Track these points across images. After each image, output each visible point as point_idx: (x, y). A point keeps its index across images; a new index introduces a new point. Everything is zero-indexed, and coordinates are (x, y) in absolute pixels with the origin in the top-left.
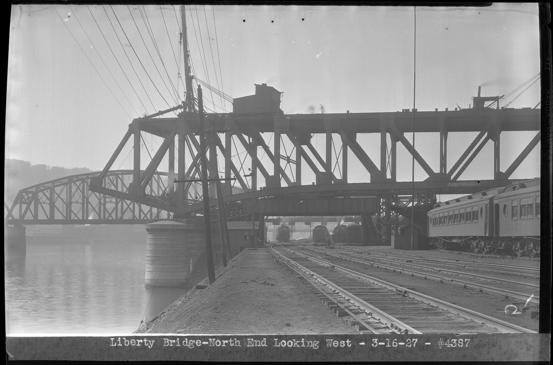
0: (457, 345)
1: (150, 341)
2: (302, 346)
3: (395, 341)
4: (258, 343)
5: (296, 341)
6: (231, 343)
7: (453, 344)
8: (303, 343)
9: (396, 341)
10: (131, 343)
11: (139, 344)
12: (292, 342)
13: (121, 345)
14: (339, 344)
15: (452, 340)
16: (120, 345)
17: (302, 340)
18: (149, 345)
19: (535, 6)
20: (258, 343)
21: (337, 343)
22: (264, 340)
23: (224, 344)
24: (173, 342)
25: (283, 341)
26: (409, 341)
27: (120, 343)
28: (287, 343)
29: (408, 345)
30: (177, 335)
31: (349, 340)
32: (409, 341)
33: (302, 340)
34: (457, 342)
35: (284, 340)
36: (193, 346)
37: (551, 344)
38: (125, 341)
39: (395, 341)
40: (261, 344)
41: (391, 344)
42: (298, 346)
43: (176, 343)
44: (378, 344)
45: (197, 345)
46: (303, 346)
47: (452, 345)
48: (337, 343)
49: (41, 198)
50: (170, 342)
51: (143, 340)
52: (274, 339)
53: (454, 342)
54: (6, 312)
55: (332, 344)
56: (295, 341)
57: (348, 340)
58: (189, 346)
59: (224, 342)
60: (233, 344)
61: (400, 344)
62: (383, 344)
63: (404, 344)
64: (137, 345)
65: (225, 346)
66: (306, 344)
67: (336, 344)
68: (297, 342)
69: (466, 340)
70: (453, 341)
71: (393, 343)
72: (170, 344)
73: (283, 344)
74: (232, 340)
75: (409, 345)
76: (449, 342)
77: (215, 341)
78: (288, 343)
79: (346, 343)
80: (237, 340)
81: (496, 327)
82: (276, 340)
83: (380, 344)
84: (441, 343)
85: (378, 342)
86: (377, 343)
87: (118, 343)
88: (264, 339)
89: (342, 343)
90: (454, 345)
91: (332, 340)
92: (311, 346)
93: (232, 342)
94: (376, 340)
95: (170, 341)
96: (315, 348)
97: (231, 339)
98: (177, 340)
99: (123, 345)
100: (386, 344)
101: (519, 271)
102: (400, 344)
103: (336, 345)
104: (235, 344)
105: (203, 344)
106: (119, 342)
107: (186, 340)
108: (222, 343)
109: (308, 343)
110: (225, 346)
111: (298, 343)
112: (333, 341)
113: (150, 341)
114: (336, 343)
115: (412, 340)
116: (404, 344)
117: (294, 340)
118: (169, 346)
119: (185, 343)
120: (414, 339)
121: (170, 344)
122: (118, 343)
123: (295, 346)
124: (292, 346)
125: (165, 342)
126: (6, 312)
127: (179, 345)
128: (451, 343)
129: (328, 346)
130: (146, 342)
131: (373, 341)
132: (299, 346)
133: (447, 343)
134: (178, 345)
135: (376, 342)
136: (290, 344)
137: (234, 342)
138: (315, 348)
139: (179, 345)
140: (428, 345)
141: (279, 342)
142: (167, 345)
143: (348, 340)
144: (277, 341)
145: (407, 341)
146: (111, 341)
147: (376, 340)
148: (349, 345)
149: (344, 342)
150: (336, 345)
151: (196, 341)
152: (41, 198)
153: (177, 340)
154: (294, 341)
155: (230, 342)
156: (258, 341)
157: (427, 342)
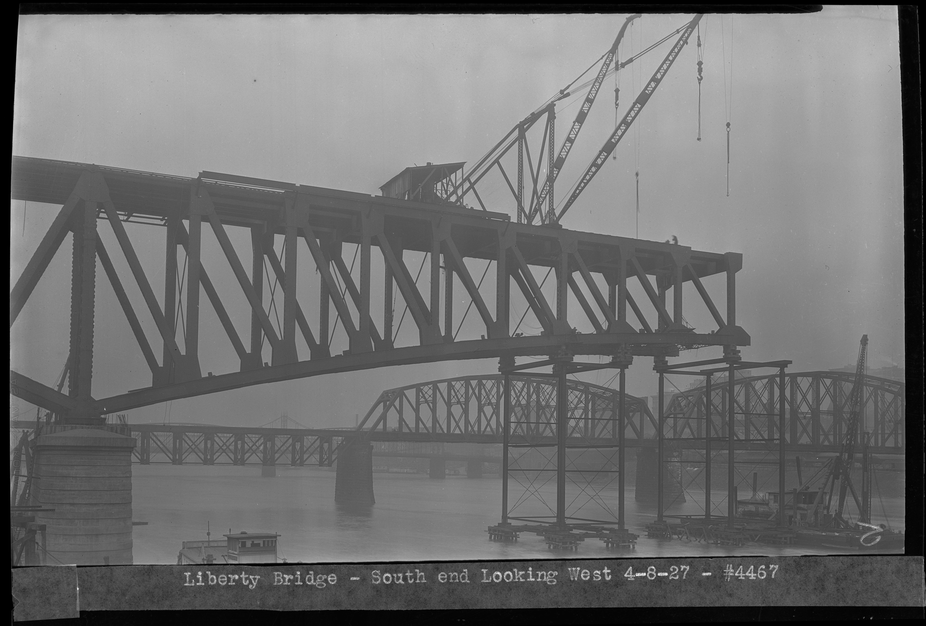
4: (542, 575)
6: (244, 580)
14: (592, 576)
18: (251, 582)
19: (893, 11)
21: (445, 576)
22: (311, 574)
23: (287, 580)
24: (235, 578)
26: (674, 570)
28: (217, 579)
31: (608, 570)
35: (497, 571)
37: (925, 571)
39: (762, 569)
40: (393, 577)
42: (522, 580)
45: (330, 582)
48: (334, 577)
49: (458, 391)
55: (579, 575)
57: (606, 568)
58: (316, 584)
60: (413, 580)
64: (198, 584)
67: (585, 575)
68: (521, 573)
69: (683, 567)
72: (284, 581)
73: (497, 577)
74: (245, 574)
75: (675, 575)
76: (752, 570)
77: (580, 572)
79: (603, 575)
84: (629, 575)
91: (578, 569)
93: (246, 579)
95: (285, 576)
96: (319, 587)
97: (243, 573)
98: (529, 570)
103: (333, 581)
109: (467, 578)
112: (580, 572)
115: (680, 568)
118: (282, 585)
122: (198, 581)
128: (681, 573)
130: (411, 576)
133: (629, 574)
134: (299, 583)
138: (319, 587)
140: (708, 577)
141: (490, 574)
143: (606, 568)
146: (186, 578)
149: (400, 575)
152: (458, 391)
156: (542, 573)
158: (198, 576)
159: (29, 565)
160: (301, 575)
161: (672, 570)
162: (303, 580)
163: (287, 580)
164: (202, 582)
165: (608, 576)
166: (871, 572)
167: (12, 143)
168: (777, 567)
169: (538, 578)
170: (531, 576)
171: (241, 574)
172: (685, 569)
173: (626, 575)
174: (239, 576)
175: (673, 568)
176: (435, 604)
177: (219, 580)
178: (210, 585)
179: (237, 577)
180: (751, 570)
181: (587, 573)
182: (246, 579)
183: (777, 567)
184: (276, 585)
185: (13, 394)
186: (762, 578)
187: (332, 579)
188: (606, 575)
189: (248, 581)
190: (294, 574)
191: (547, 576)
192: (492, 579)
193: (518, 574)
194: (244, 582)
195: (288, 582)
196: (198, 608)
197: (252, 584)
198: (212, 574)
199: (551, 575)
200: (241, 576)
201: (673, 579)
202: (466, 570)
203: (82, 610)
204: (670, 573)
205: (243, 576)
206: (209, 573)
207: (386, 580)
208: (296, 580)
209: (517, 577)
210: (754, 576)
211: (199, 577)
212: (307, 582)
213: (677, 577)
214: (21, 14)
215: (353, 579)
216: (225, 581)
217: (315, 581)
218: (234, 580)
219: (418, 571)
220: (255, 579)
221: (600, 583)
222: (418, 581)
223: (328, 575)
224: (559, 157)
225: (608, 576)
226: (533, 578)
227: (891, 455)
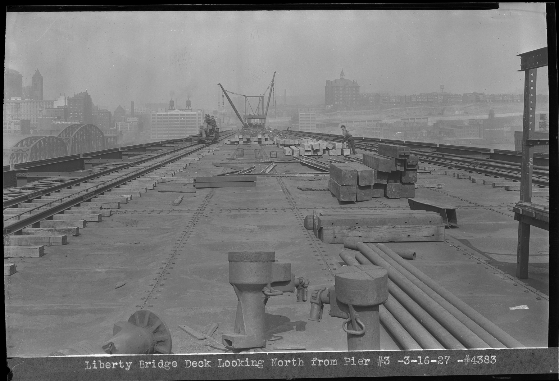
1: (127, 363)
5: (207, 360)
6: (121, 365)
8: (420, 359)
10: (193, 364)
13: (96, 368)
15: (478, 357)
16: (95, 368)
17: (352, 358)
21: (195, 363)
25: (228, 361)
31: (295, 360)
32: (441, 358)
33: (352, 358)
34: (483, 358)
36: (169, 368)
39: (427, 359)
40: (330, 362)
42: (242, 366)
43: (352, 362)
46: (248, 365)
48: (195, 363)
50: (145, 364)
51: (118, 363)
53: (494, 359)
56: (239, 361)
59: (114, 364)
61: (432, 361)
62: (416, 361)
64: (112, 368)
66: (250, 363)
68: (208, 362)
69: (446, 357)
71: (425, 361)
72: (145, 366)
73: (227, 364)
77: (277, 361)
80: (300, 360)
82: (220, 360)
83: (412, 361)
85: (410, 359)
86: (409, 360)
90: (407, 362)
92: (256, 365)
94: (408, 357)
100: (418, 362)
101: (429, 290)
102: (432, 361)
103: (194, 365)
105: (431, 362)
106: (94, 365)
107: (161, 362)
108: (285, 363)
111: (243, 363)
113: (127, 363)
115: (444, 357)
119: (160, 365)
120: (493, 356)
123: (239, 366)
128: (444, 361)
131: (405, 358)
136: (234, 364)
139: (249, 366)
142: (428, 363)
144: (88, 363)
147: (408, 357)
148: (295, 364)
150: (194, 365)
151: (171, 363)
157: (432, 360)
158: (93, 363)
159: (12, 357)
161: (439, 358)
162: (156, 365)
163: (366, 362)
164: (96, 367)
166: (517, 361)
167: (526, 2)
168: (449, 357)
171: (119, 362)
172: (447, 358)
174: (291, 361)
175: (440, 358)
176: (343, 375)
177: (106, 365)
179: (116, 364)
180: (474, 359)
182: (122, 365)
183: (449, 357)
184: (87, 370)
185: (547, 217)
195: (367, 363)
196: (276, 378)
198: (101, 362)
199: (167, 364)
202: (495, 356)
204: (438, 360)
208: (152, 364)
209: (239, 364)
211: (408, 360)
212: (425, 363)
213: (443, 363)
214: (8, 12)
216: (109, 366)
218: (148, 365)
219: (299, 358)
220: (129, 364)
224: (200, 144)
226: (96, 367)
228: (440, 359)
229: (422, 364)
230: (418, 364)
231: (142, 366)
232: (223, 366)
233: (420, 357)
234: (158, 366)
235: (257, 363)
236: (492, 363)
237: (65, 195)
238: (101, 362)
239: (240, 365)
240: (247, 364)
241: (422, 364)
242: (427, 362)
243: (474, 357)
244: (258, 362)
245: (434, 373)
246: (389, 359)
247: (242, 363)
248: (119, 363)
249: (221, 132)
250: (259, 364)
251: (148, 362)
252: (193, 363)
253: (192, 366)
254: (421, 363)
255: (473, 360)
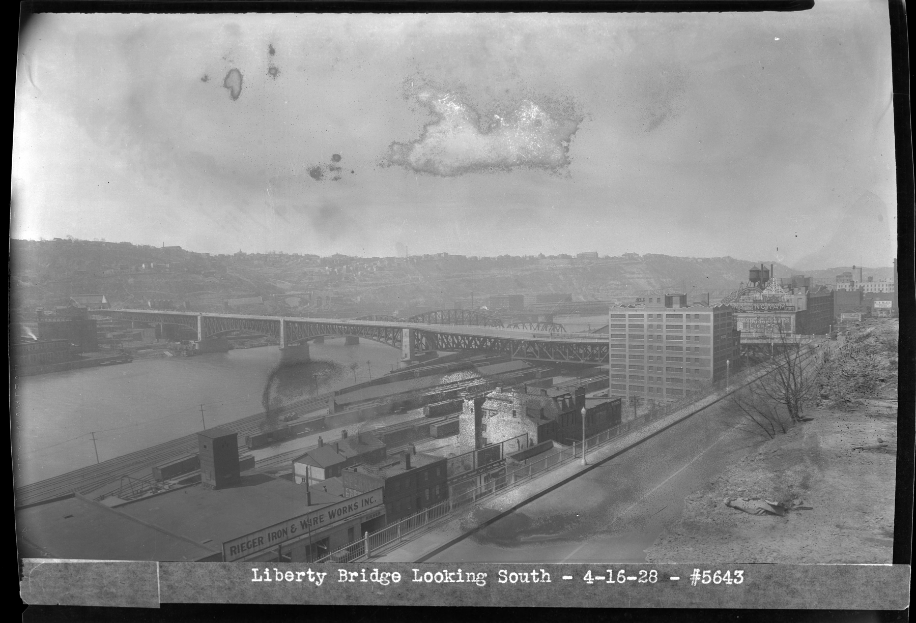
0: (508, 581)
1: (318, 574)
2: (458, 581)
3: (717, 574)
4: (471, 576)
7: (737, 578)
9: (720, 575)
11: (352, 578)
12: (292, 575)
16: (268, 580)
18: (317, 579)
20: (471, 576)
27: (364, 577)
28: (284, 575)
29: (642, 579)
30: (77, 560)
32: (644, 574)
33: (458, 572)
36: (387, 582)
38: (277, 573)
40: (519, 576)
41: (614, 578)
42: (452, 581)
43: (360, 577)
44: (626, 578)
47: (735, 581)
50: (349, 576)
52: (413, 570)
54: (234, 30)
58: (380, 581)
60: (538, 580)
62: (603, 578)
63: (635, 578)
64: (265, 580)
65: (353, 581)
66: (464, 577)
68: (451, 574)
70: (738, 574)
72: (349, 578)
73: (428, 577)
76: (729, 576)
78: (435, 577)
79: (530, 578)
81: (890, 405)
83: (629, 578)
87: (265, 577)
88: (375, 570)
89: (503, 573)
92: (474, 581)
98: (362, 572)
99: (274, 579)
100: (608, 578)
104: (541, 579)
109: (468, 577)
110: (353, 581)
111: (452, 577)
113: (318, 574)
114: (397, 577)
116: (635, 578)
117: (444, 571)
119: (374, 577)
121: (349, 578)
122: (265, 577)
124: (443, 581)
125: (341, 575)
126: (234, 30)
127: (366, 579)
129: (692, 584)
132: (454, 581)
135: (740, 576)
136: (439, 578)
137: (540, 576)
142: (514, 580)
143: (310, 570)
145: (641, 573)
148: (536, 580)
149: (526, 574)
153: (362, 572)
154: (445, 573)
155: (592, 578)
156: (471, 574)
158: (265, 573)
160: (462, 573)
162: (367, 577)
164: (462, 579)
165: (312, 577)
169: (472, 579)
170: (611, 579)
173: (585, 579)
174: (306, 573)
175: (642, 572)
178: (277, 581)
179: (303, 574)
181: (290, 574)
186: (655, 582)
187: (397, 577)
188: (310, 576)
189: (314, 578)
190: (359, 572)
191: (476, 577)
192: (423, 579)
193: (448, 576)
194: (484, 585)
196: (287, 604)
197: (319, 581)
198: (545, 572)
200: (532, 574)
201: (641, 582)
203: (165, 602)
204: (639, 576)
205: (310, 572)
206: (276, 569)
207: (372, 577)
209: (447, 578)
210: (730, 581)
215: (565, 578)
217: (379, 579)
220: (321, 576)
221: (624, 585)
222: (469, 581)
223: (391, 573)
225: (312, 577)
226: (462, 579)
227: (337, 525)
228: (642, 576)
229: (614, 582)
230: (608, 582)
231: (343, 578)
232: (421, 580)
233: (610, 571)
234: (616, 580)
235: (476, 577)
236: (737, 583)
237: (147, 477)
238: (545, 572)
239: (449, 580)
240: (254, 577)
241: (614, 582)
242: (621, 579)
243: (728, 573)
244: (478, 575)
245: (469, 602)
246: (743, 575)
247: (451, 577)
248: (307, 573)
249: (257, 462)
250: (382, 579)
251: (352, 572)
252: (286, 574)
253: (434, 580)
254: (611, 581)
255: (727, 578)
